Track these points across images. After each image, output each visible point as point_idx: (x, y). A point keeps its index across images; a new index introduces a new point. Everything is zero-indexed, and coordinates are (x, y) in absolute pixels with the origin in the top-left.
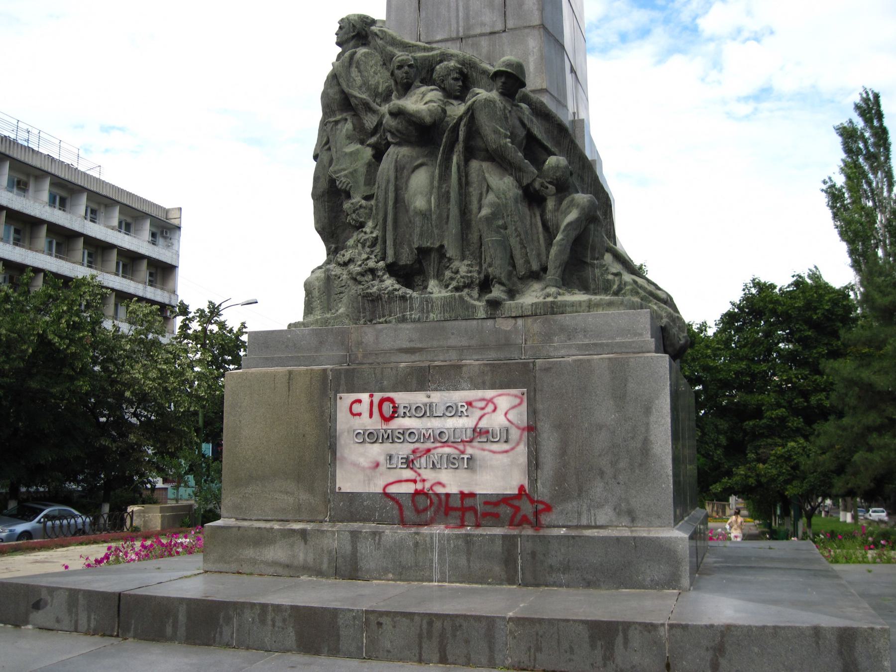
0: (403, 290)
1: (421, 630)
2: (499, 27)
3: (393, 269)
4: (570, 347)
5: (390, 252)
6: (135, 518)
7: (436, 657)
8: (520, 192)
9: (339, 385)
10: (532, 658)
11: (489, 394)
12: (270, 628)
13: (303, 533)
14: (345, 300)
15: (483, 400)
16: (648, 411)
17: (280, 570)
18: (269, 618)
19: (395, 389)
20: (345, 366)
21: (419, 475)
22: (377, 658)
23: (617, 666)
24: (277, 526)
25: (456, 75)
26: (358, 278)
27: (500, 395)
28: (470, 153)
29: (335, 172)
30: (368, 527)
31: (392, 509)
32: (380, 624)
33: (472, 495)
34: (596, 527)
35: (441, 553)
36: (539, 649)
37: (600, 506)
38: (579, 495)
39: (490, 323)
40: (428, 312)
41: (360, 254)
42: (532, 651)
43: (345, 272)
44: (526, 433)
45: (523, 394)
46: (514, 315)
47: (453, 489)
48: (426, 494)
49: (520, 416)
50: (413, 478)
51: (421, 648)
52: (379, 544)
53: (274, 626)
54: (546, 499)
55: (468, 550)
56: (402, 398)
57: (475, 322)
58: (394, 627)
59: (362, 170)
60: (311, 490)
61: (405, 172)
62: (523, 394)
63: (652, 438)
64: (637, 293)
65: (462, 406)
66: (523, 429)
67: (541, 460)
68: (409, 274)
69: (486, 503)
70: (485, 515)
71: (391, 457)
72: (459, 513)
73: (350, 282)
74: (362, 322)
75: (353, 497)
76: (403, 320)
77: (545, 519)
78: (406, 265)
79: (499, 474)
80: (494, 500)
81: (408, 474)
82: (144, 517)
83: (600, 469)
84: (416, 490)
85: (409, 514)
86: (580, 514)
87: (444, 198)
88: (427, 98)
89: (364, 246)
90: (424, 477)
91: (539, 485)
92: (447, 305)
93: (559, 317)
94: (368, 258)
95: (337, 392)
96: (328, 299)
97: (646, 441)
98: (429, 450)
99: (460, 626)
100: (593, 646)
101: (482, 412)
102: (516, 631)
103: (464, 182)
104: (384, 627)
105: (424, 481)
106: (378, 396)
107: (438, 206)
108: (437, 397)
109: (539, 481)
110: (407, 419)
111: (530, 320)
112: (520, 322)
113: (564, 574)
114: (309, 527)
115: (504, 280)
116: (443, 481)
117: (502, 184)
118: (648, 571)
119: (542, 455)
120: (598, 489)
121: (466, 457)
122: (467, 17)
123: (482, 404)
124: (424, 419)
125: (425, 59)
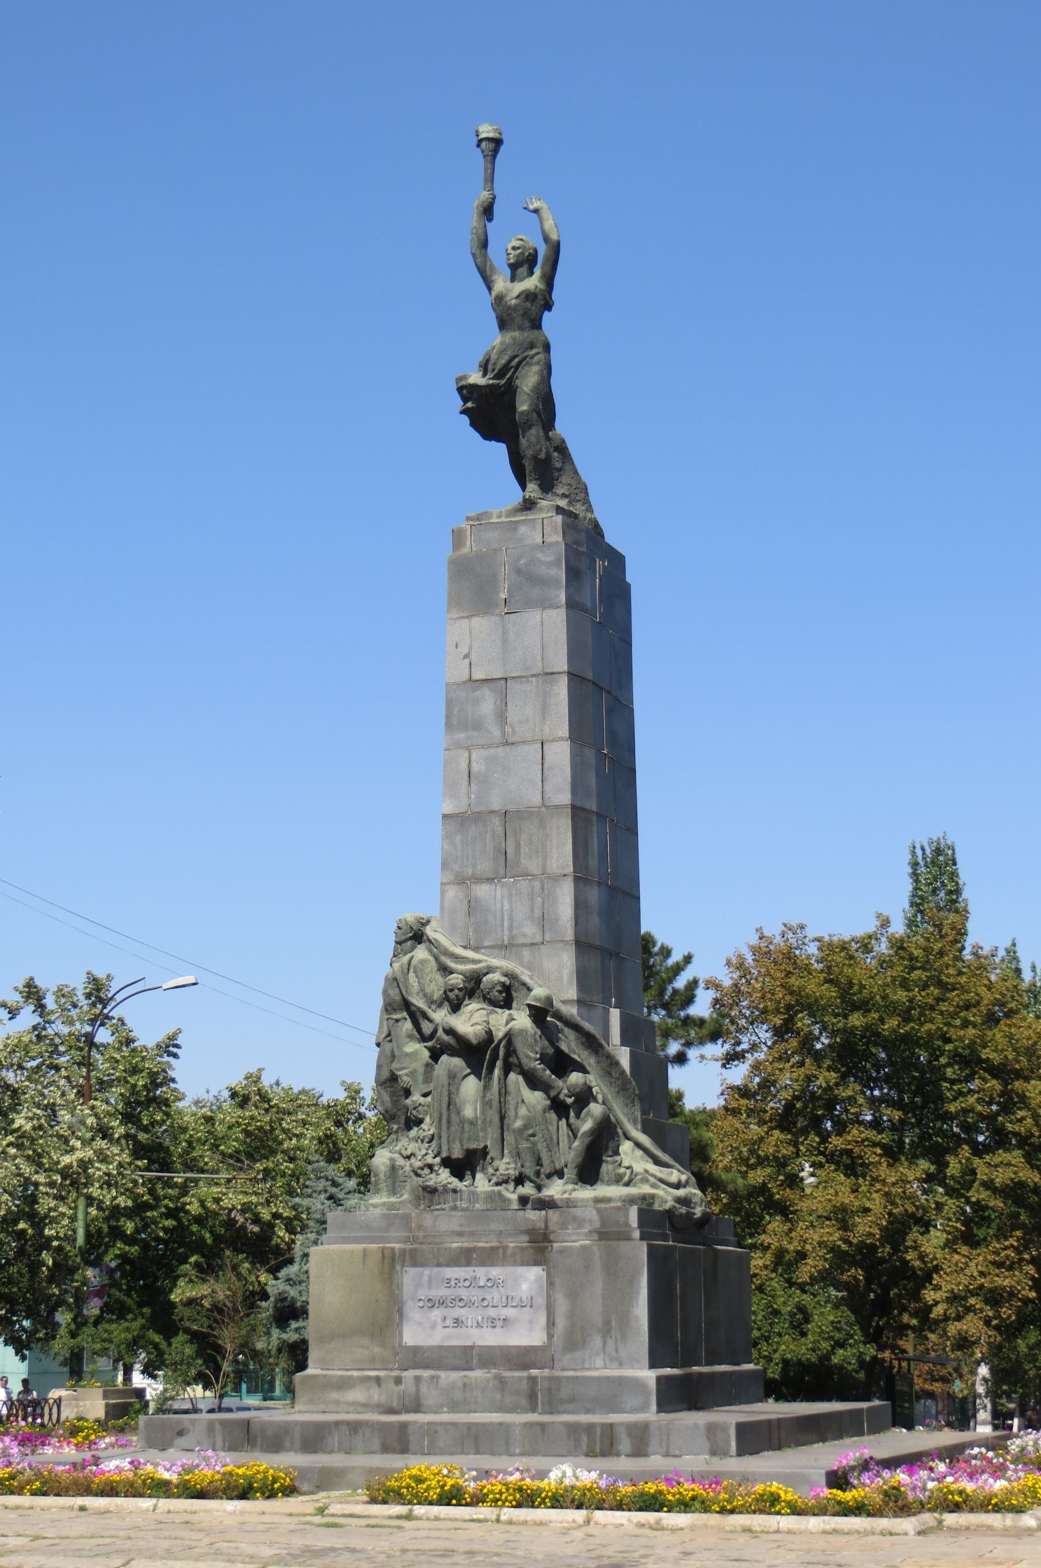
0: (455, 1182)
2: (538, 939)
3: (447, 1163)
4: (580, 1234)
5: (445, 1148)
6: (62, 1408)
8: (548, 1102)
9: (404, 1261)
13: (378, 1380)
14: (408, 1187)
17: (359, 1409)
20: (408, 1246)
22: (435, 1454)
24: (356, 1374)
25: (499, 988)
26: (419, 1171)
28: (507, 1070)
29: (397, 1070)
30: (426, 1373)
39: (521, 1213)
41: (420, 1150)
43: (408, 1164)
59: (421, 1070)
60: (383, 1345)
61: (457, 1081)
64: (648, 1181)
68: (463, 1166)
73: (412, 1174)
74: (422, 1207)
75: (416, 1350)
76: (455, 1208)
79: (528, 1333)
82: (77, 1406)
87: (486, 1104)
88: (473, 1021)
89: (422, 1141)
92: (490, 1197)
93: (572, 1210)
94: (426, 1154)
95: (403, 1266)
96: (394, 1183)
103: (504, 1091)
107: (483, 1112)
114: (382, 1373)
117: (536, 1099)
122: (511, 927)
125: (474, 971)
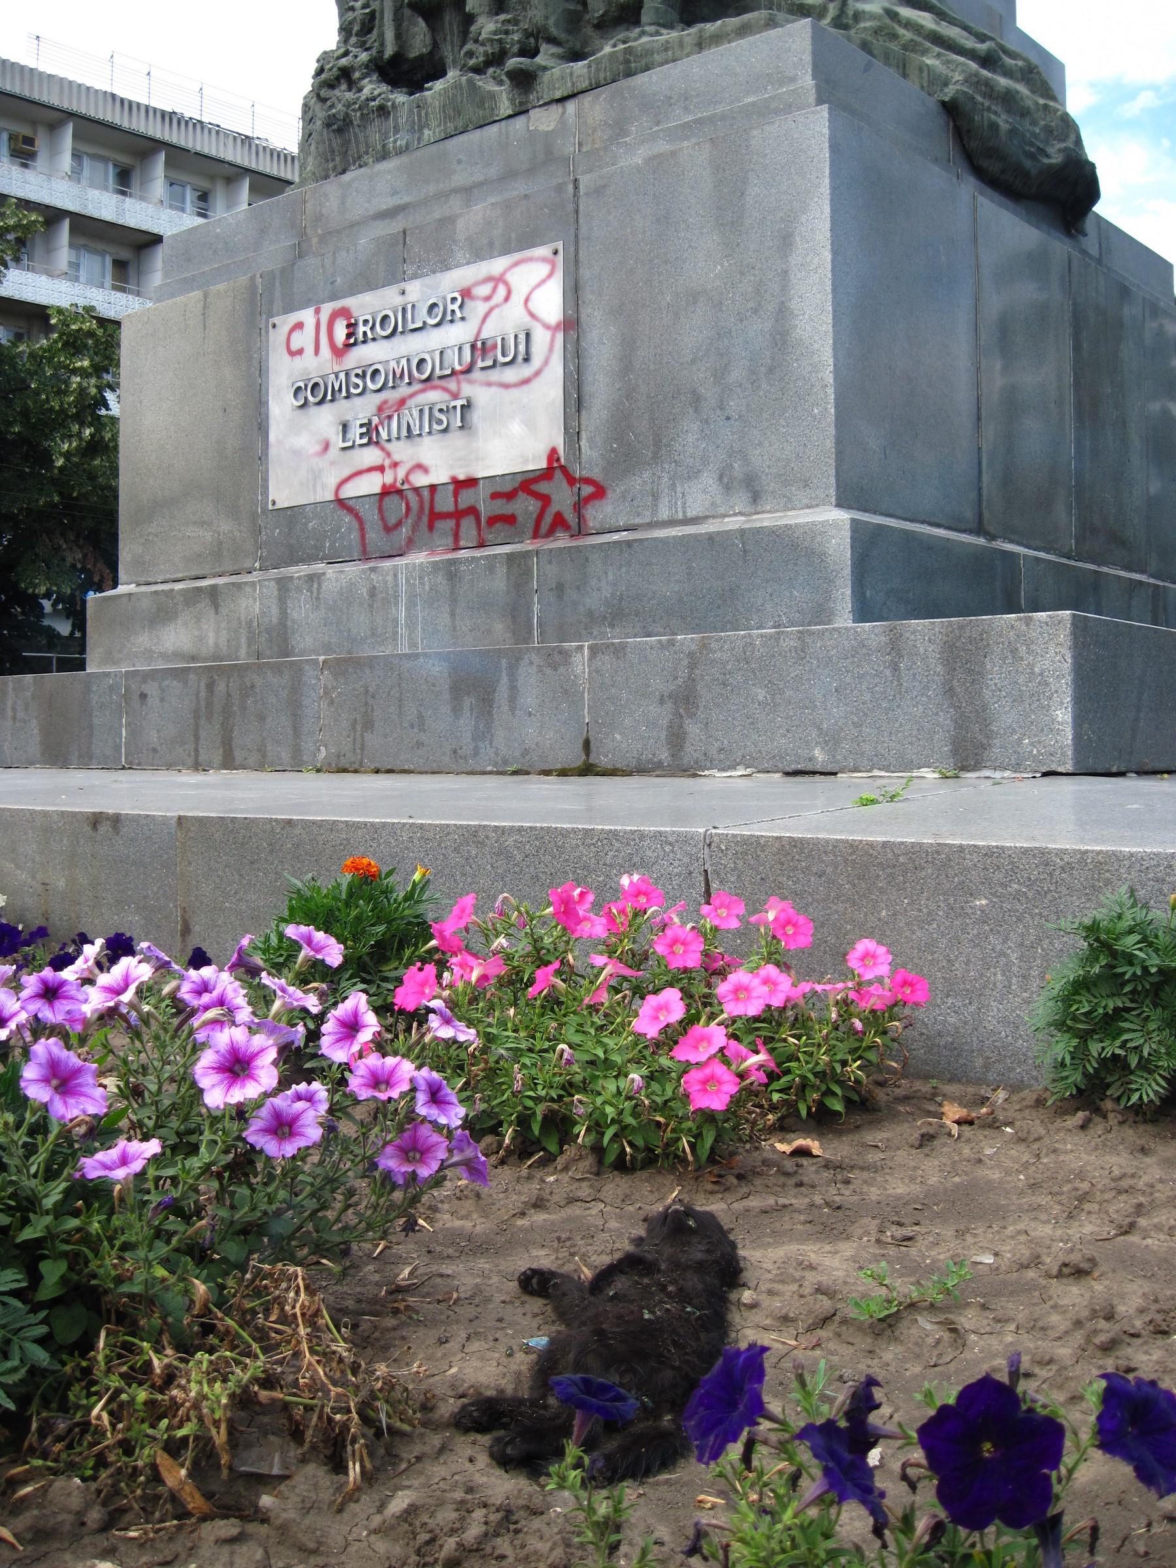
1: (198, 702)
7: (218, 758)
10: (359, 741)
11: (497, 265)
12: (9, 723)
15: (489, 279)
16: (786, 242)
18: (9, 703)
19: (352, 291)
21: (388, 455)
23: (497, 754)
27: (516, 264)
30: (299, 571)
31: (350, 529)
32: (143, 696)
33: (471, 482)
34: (687, 522)
35: (411, 605)
36: (369, 725)
37: (693, 474)
38: (656, 456)
40: (421, 129)
42: (359, 728)
44: (560, 337)
45: (556, 253)
46: (558, 95)
47: (440, 476)
48: (400, 492)
49: (550, 303)
50: (379, 462)
51: (197, 738)
52: (318, 599)
53: (14, 718)
54: (596, 474)
55: (452, 593)
56: (365, 305)
57: (494, 128)
58: (162, 700)
62: (556, 253)
63: (794, 305)
65: (454, 300)
66: (555, 329)
67: (587, 389)
69: (495, 496)
70: (492, 521)
71: (345, 427)
72: (451, 523)
76: (384, 156)
77: (596, 514)
78: (421, 58)
80: (508, 488)
81: (372, 456)
83: (694, 392)
84: (384, 486)
85: (374, 535)
86: (656, 497)
90: (396, 457)
91: (583, 443)
93: (641, 79)
95: (271, 315)
97: (783, 312)
98: (402, 402)
99: (253, 686)
100: (456, 711)
101: (487, 306)
102: (334, 688)
104: (150, 700)
105: (395, 465)
106: (327, 309)
108: (417, 291)
109: (584, 435)
110: (371, 346)
111: (587, 99)
112: (571, 106)
113: (612, 626)
115: (554, 31)
116: (425, 461)
118: (769, 607)
119: (588, 377)
120: (691, 438)
121: (459, 403)
123: (484, 290)
124: (397, 340)
